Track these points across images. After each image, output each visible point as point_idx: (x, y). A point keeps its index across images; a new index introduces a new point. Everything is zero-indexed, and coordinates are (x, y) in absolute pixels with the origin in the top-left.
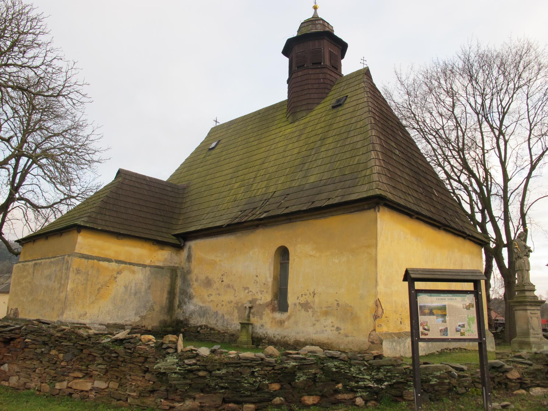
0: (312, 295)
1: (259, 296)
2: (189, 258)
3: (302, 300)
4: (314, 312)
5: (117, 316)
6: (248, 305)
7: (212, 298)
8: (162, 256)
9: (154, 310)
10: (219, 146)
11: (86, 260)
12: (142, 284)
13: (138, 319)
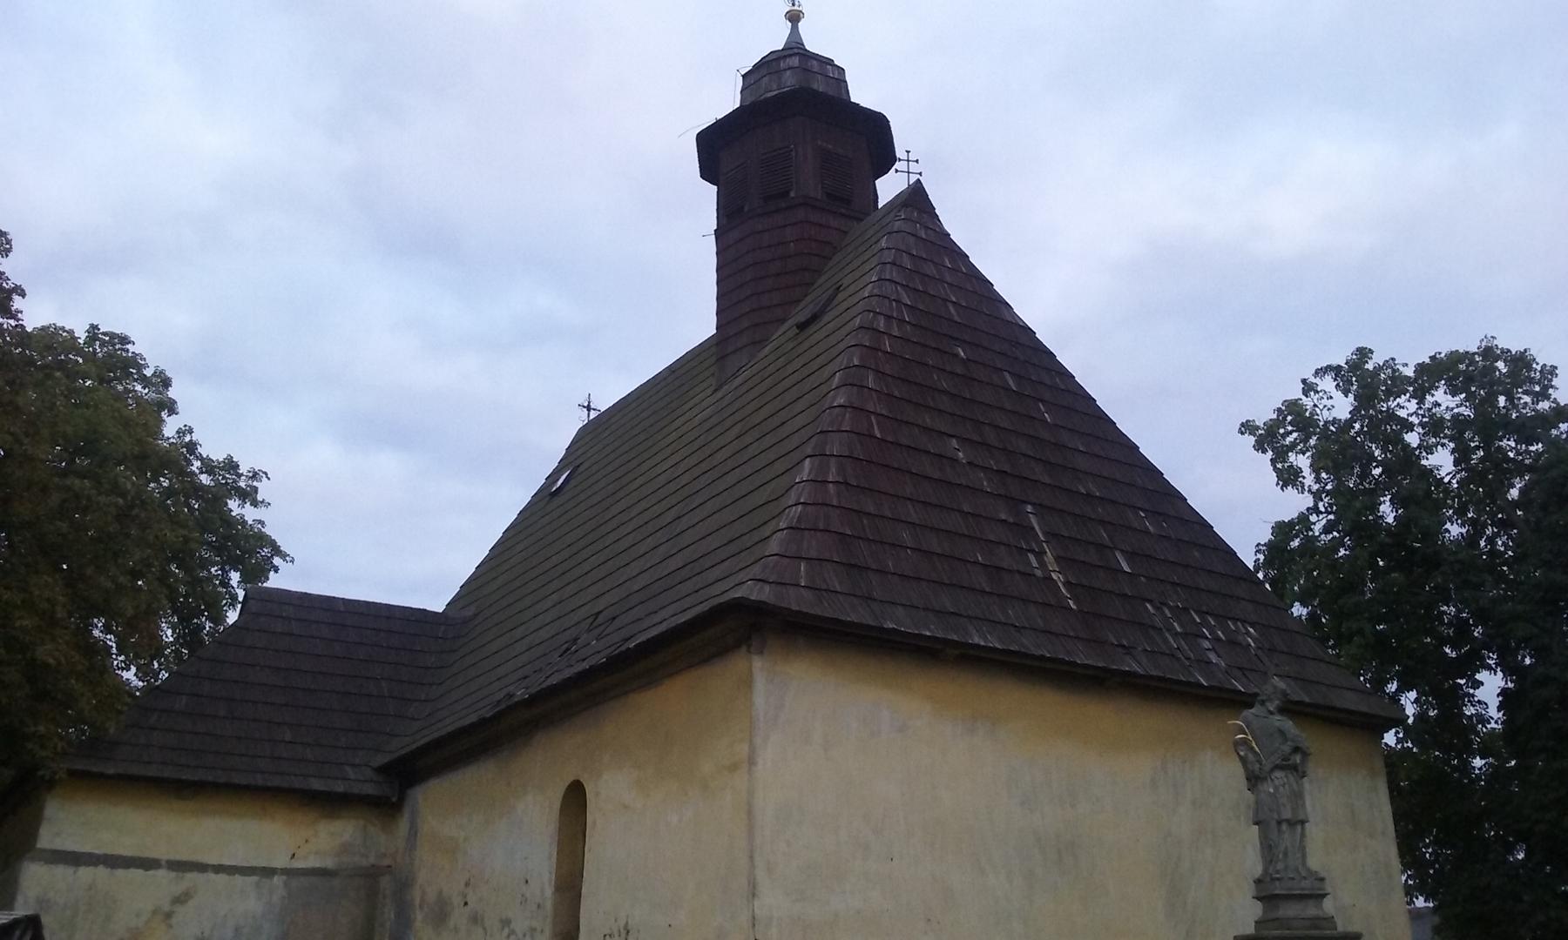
0: (623, 933)
2: (413, 832)
8: (317, 842)
10: (573, 483)
11: (70, 870)
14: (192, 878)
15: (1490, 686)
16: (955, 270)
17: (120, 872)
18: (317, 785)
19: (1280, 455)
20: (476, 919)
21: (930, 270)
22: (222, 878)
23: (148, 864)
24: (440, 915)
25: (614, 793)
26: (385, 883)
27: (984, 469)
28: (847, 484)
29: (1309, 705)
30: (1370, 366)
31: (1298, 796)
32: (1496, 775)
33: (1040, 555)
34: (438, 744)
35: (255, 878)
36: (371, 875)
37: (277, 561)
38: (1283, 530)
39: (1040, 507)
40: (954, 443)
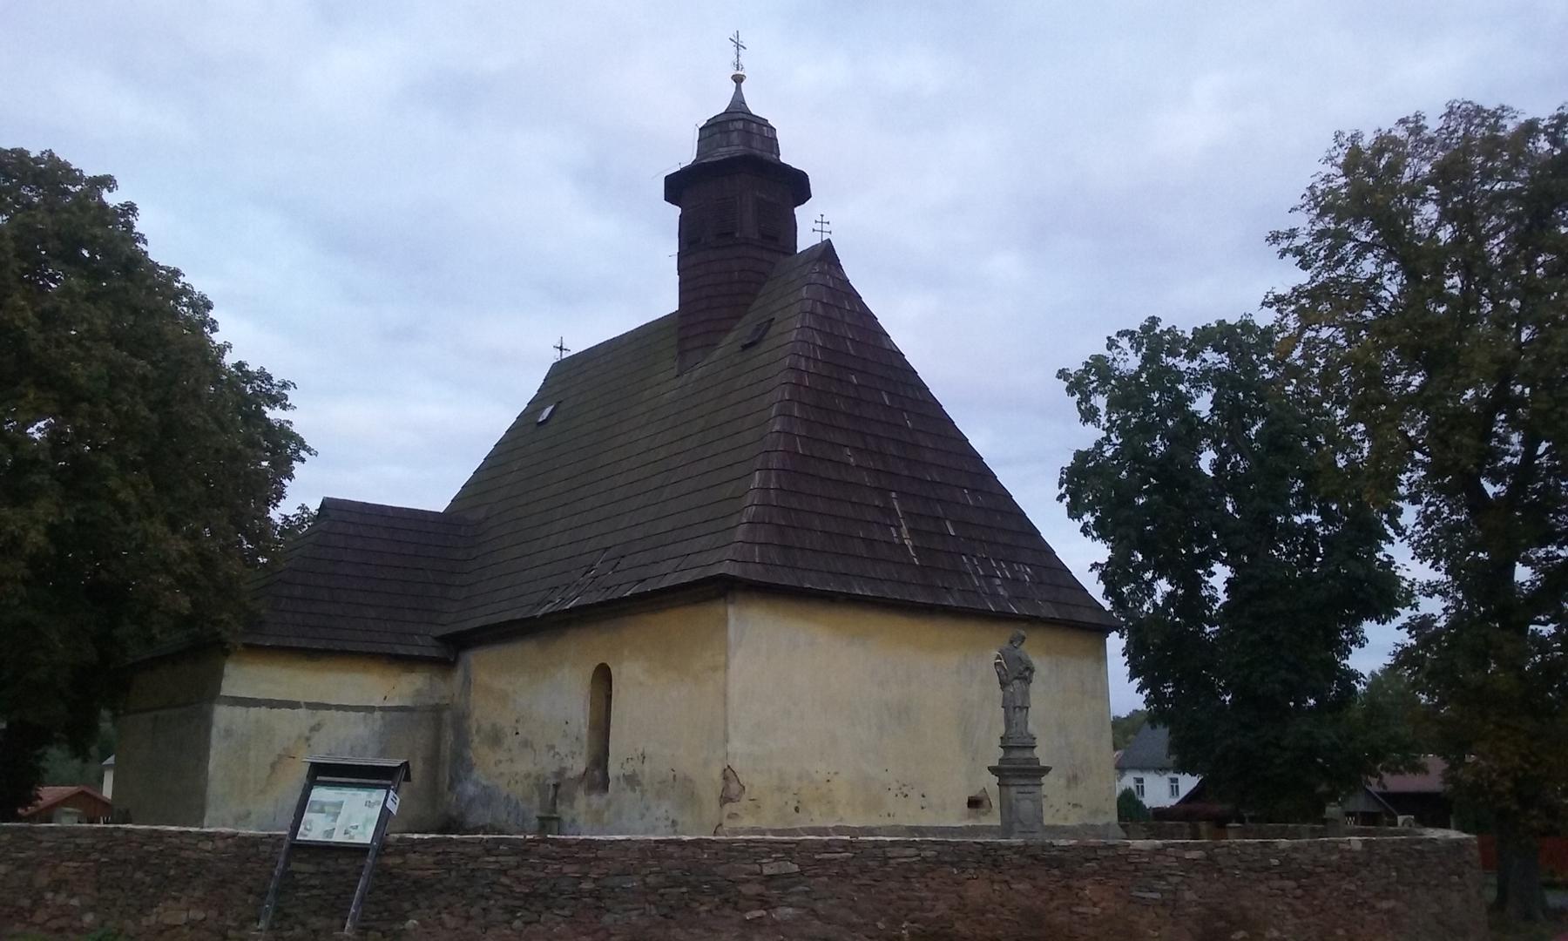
1: (568, 763)
2: (467, 682)
3: (628, 769)
4: (643, 792)
6: (552, 781)
7: (503, 768)
11: (244, 710)
15: (1220, 576)
16: (852, 311)
17: (275, 711)
18: (401, 651)
19: (1085, 398)
20: (526, 744)
21: (836, 314)
23: (293, 705)
24: (495, 739)
25: (629, 674)
26: (447, 715)
27: (867, 469)
28: (781, 489)
30: (1157, 331)
31: (1026, 694)
32: (1222, 638)
33: (898, 528)
34: (484, 628)
36: (437, 710)
37: (303, 453)
38: (1081, 457)
39: (902, 495)
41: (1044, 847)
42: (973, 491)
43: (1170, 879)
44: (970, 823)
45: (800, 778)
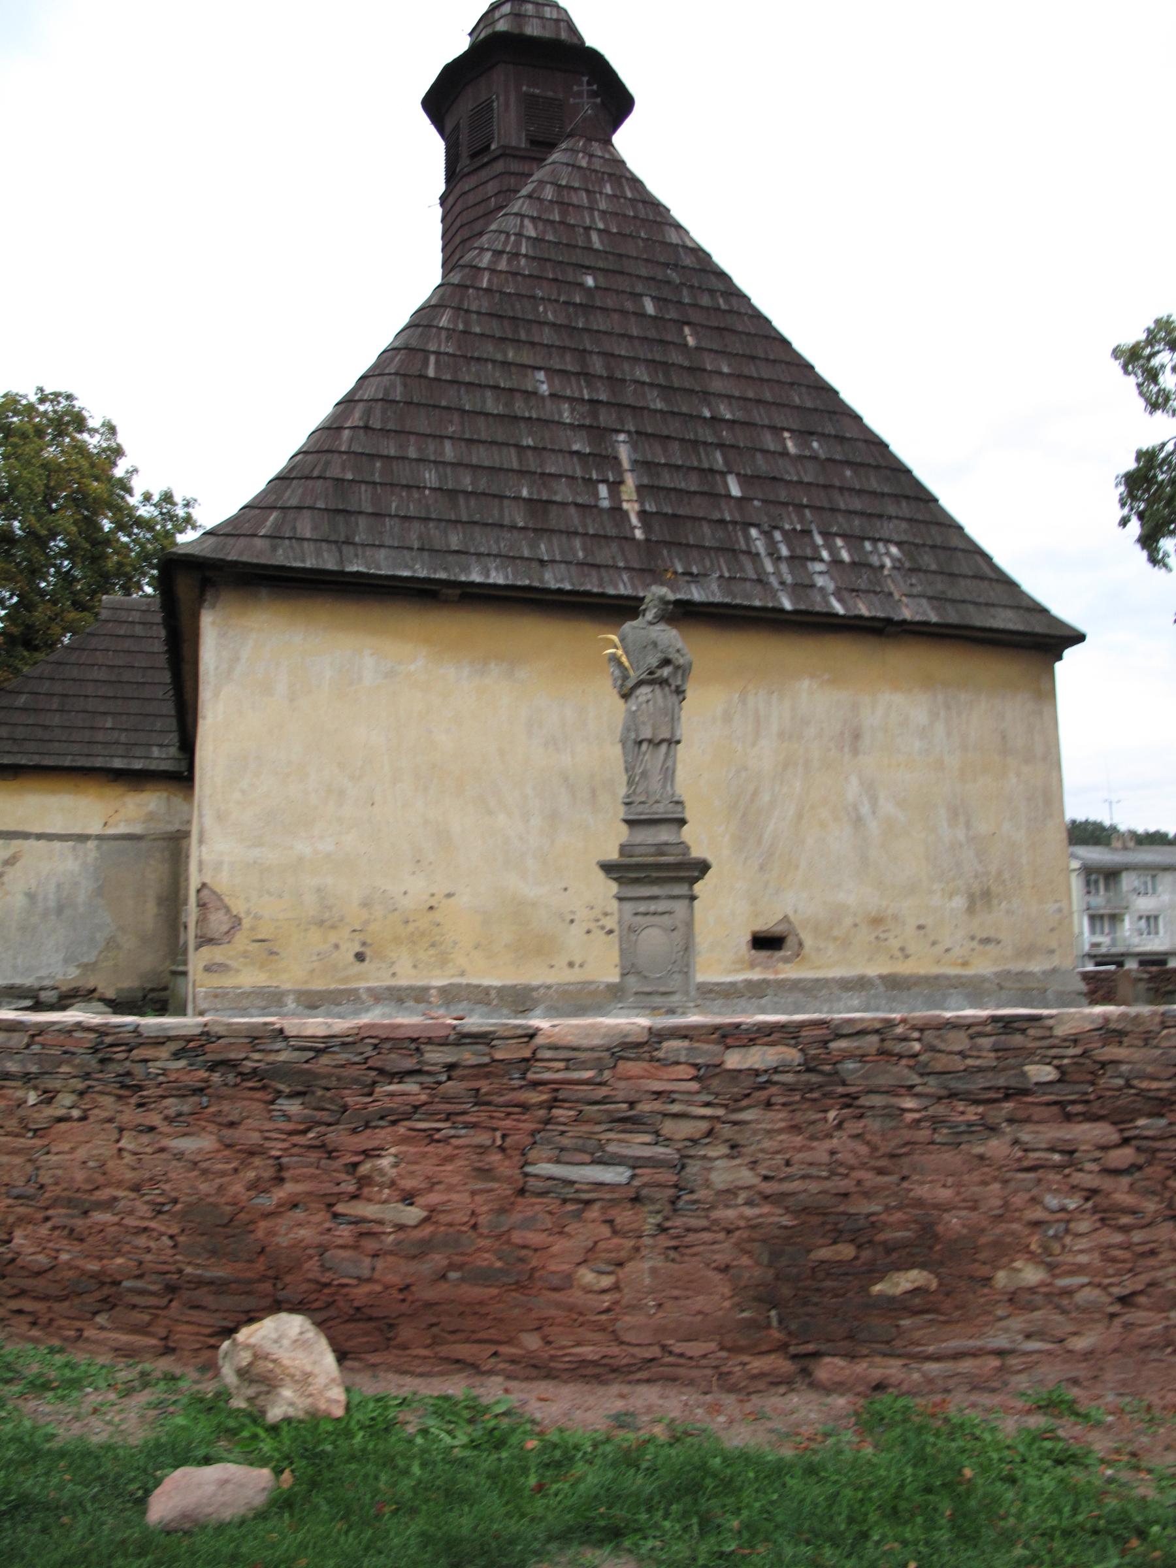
5: (14, 967)
9: (119, 947)
12: (76, 884)
13: (73, 972)
14: (17, 844)
18: (118, 764)
22: (42, 843)
29: (936, 625)
33: (615, 487)
35: (71, 843)
39: (639, 437)
40: (541, 375)
41: (255, 1038)
42: (805, 435)
43: (668, 1127)
44: (755, 975)
45: (366, 904)
